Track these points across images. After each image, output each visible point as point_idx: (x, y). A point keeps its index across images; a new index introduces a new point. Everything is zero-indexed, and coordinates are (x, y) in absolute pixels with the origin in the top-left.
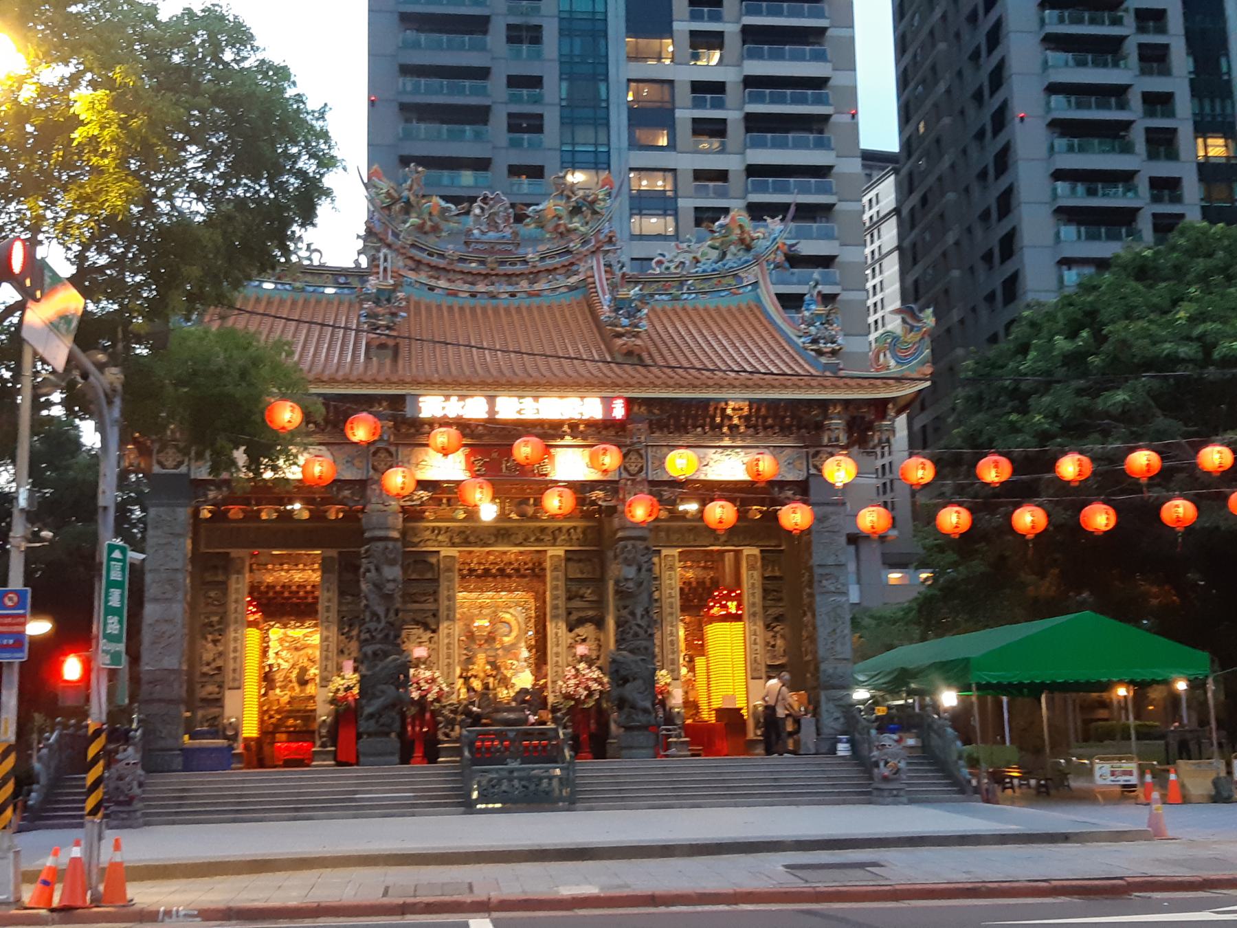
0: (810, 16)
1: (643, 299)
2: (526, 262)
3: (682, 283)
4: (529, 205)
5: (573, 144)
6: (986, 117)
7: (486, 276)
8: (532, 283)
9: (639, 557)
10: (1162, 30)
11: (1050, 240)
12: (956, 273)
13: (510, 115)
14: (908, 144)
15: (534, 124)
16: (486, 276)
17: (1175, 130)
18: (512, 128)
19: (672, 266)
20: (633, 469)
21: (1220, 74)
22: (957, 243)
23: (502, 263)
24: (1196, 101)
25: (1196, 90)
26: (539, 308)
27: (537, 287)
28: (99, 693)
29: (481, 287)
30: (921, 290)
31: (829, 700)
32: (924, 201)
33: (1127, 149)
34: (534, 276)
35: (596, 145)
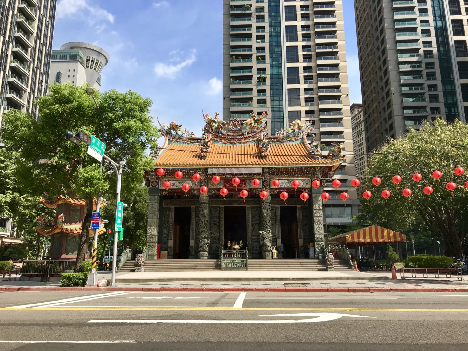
0: (335, 70)
1: (269, 142)
2: (243, 135)
3: (283, 139)
4: (244, 121)
5: (274, 106)
6: (384, 94)
7: (234, 139)
8: (245, 140)
9: (267, 207)
10: (433, 68)
11: (402, 125)
12: (378, 135)
13: (258, 100)
14: (364, 101)
15: (264, 101)
16: (234, 139)
17: (438, 94)
18: (258, 103)
19: (281, 134)
20: (266, 185)
21: (450, 78)
22: (378, 127)
23: (238, 135)
24: (444, 86)
25: (444, 83)
26: (363, 153)
27: (246, 141)
28: (325, 296)
29: (232, 141)
30: (369, 139)
31: (317, 244)
32: (369, 116)
33: (424, 100)
34: (245, 139)
35: (280, 106)
